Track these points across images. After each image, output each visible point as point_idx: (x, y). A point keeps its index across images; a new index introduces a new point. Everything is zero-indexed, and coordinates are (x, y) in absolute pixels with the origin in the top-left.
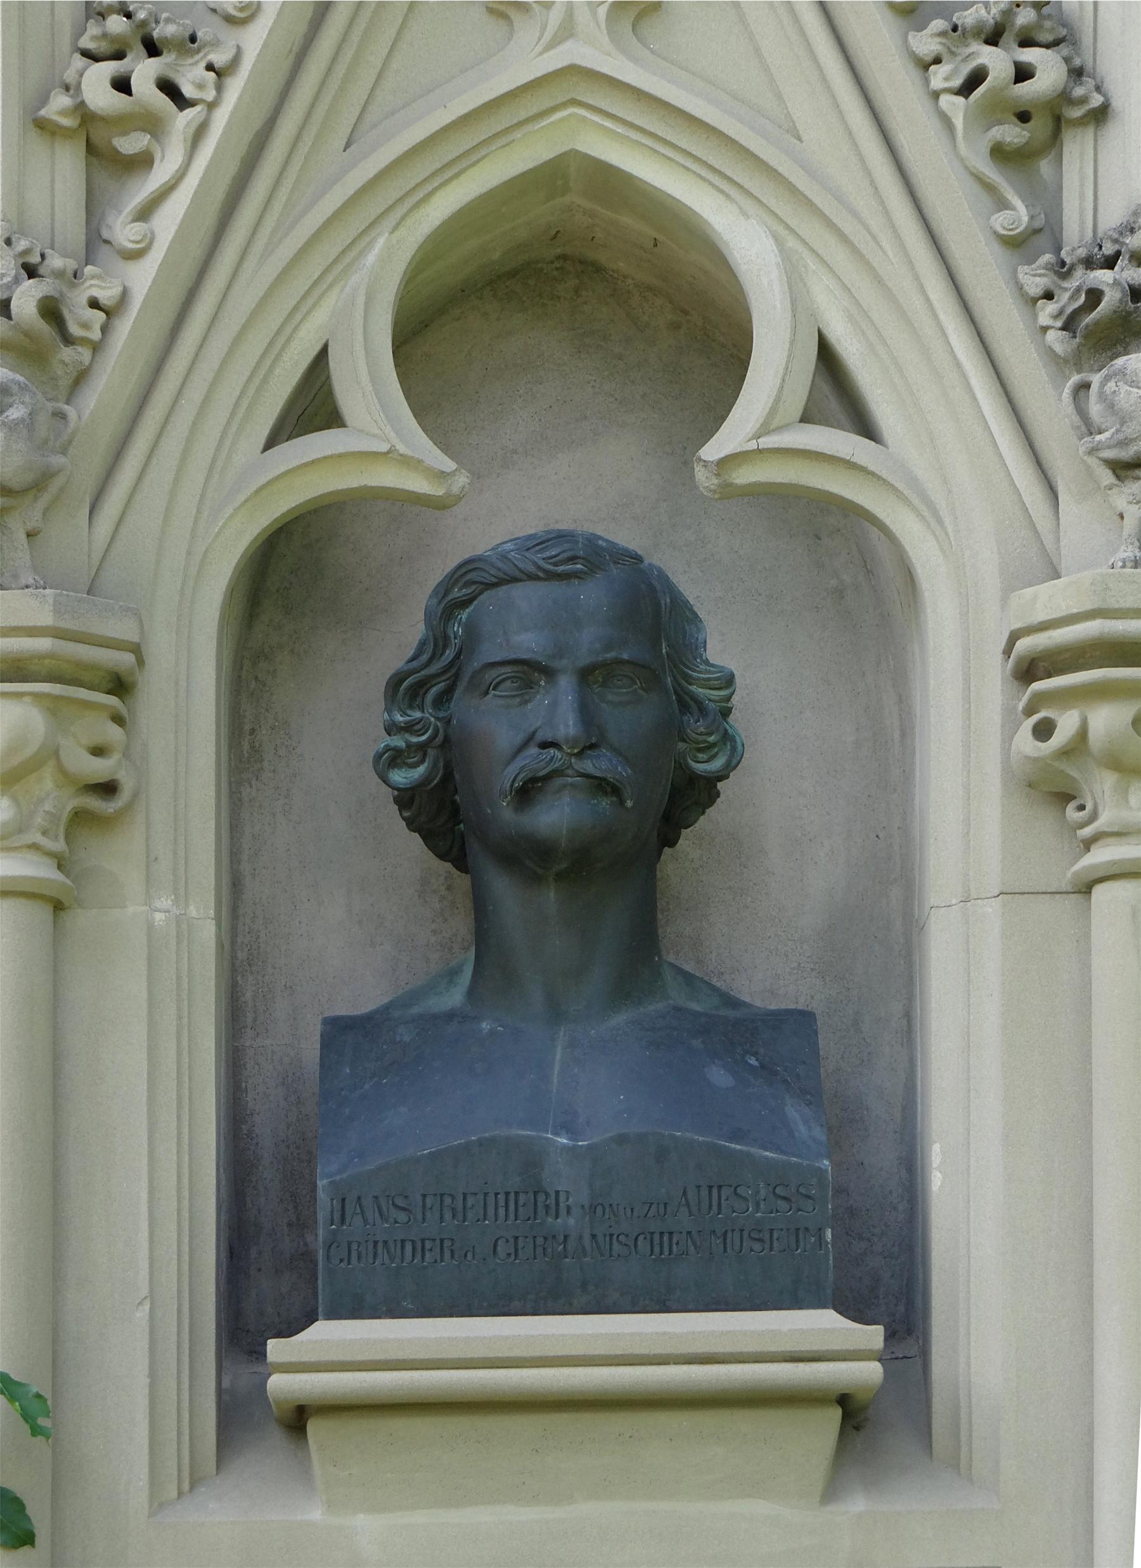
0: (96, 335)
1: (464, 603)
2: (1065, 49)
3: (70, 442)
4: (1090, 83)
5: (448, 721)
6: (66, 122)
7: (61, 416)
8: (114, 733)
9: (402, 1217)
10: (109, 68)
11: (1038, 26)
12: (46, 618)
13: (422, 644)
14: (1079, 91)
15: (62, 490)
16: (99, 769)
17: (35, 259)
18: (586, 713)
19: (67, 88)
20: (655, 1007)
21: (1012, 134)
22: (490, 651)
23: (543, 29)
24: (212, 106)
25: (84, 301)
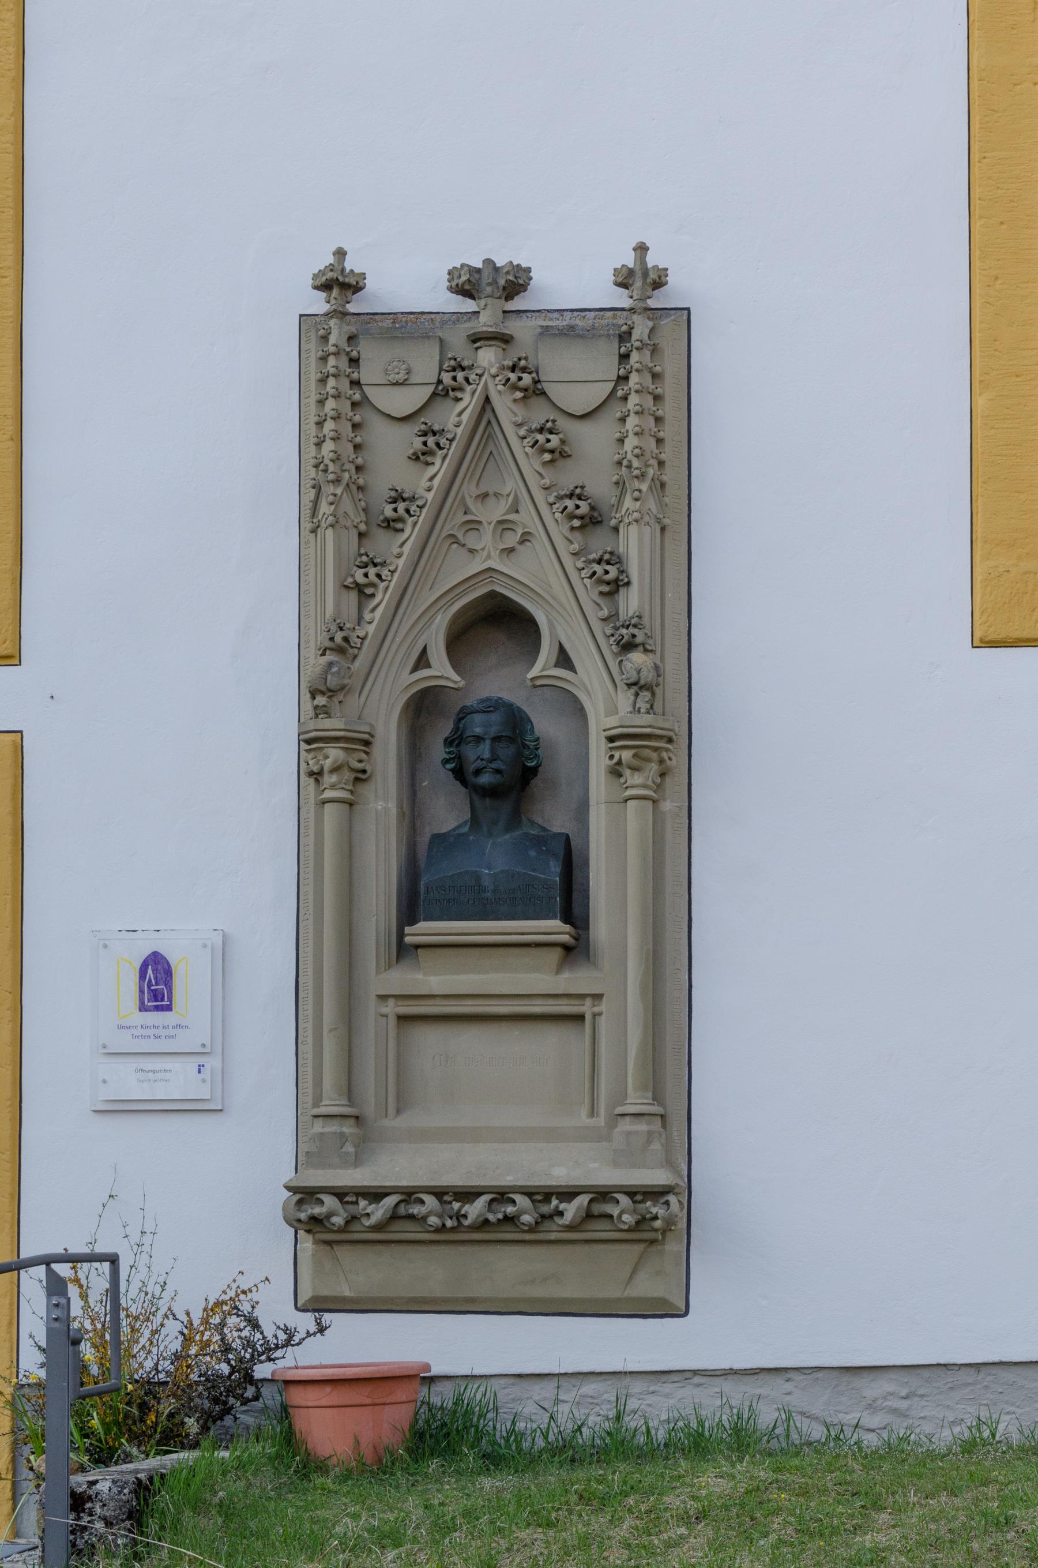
0: (359, 646)
1: (463, 718)
2: (618, 566)
3: (352, 675)
4: (625, 575)
5: (459, 751)
6: (352, 586)
7: (349, 668)
8: (363, 756)
9: (443, 892)
10: (363, 571)
11: (611, 559)
12: (342, 727)
13: (453, 729)
14: (621, 578)
15: (349, 690)
16: (360, 766)
17: (342, 625)
18: (493, 751)
19: (352, 576)
20: (518, 833)
21: (606, 589)
22: (468, 733)
23: (482, 557)
24: (390, 581)
25: (355, 636)
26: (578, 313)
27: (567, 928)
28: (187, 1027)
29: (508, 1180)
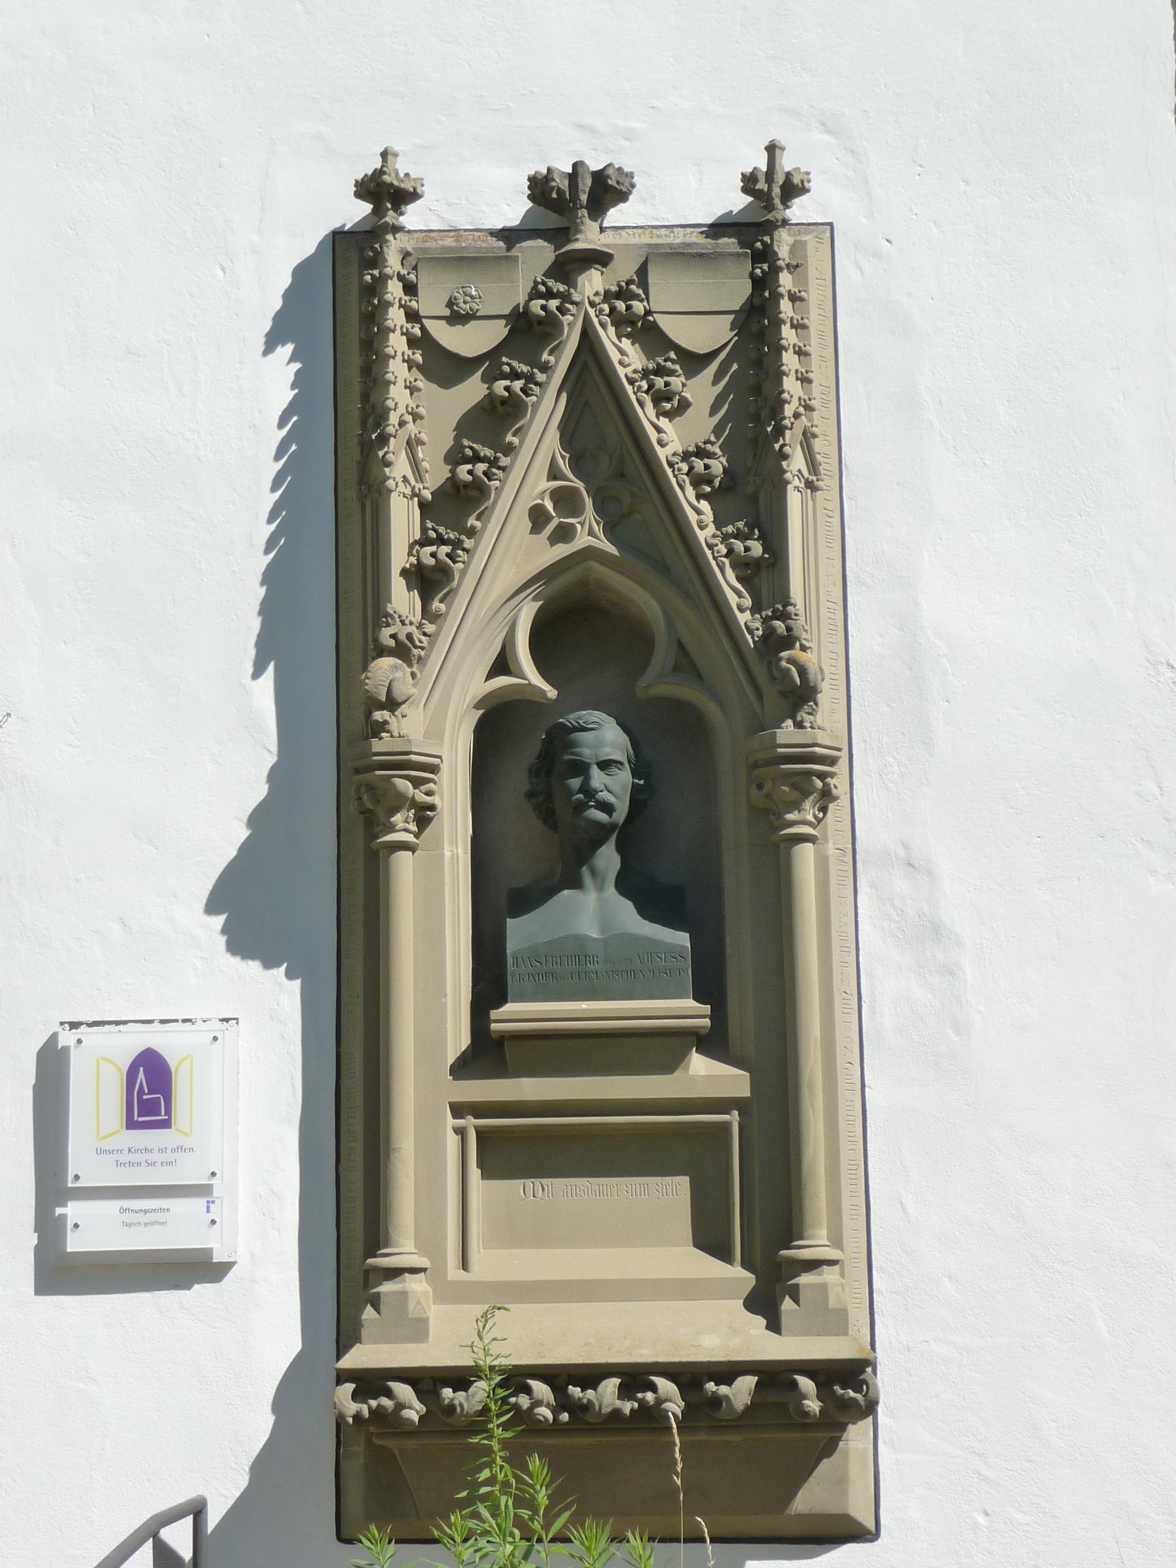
26: (691, 230)
27: (706, 1009)
28: (191, 1150)
29: (644, 1354)
